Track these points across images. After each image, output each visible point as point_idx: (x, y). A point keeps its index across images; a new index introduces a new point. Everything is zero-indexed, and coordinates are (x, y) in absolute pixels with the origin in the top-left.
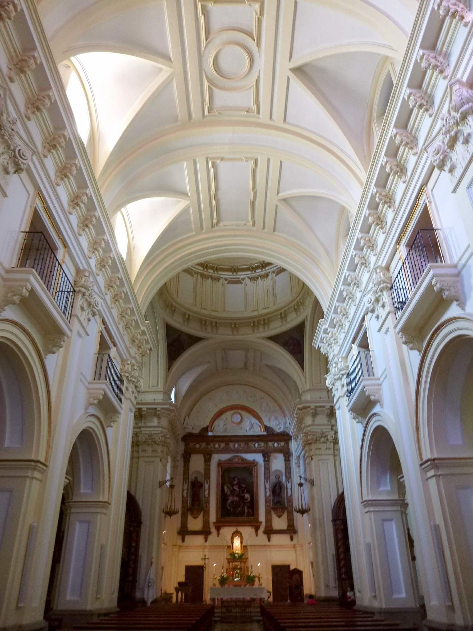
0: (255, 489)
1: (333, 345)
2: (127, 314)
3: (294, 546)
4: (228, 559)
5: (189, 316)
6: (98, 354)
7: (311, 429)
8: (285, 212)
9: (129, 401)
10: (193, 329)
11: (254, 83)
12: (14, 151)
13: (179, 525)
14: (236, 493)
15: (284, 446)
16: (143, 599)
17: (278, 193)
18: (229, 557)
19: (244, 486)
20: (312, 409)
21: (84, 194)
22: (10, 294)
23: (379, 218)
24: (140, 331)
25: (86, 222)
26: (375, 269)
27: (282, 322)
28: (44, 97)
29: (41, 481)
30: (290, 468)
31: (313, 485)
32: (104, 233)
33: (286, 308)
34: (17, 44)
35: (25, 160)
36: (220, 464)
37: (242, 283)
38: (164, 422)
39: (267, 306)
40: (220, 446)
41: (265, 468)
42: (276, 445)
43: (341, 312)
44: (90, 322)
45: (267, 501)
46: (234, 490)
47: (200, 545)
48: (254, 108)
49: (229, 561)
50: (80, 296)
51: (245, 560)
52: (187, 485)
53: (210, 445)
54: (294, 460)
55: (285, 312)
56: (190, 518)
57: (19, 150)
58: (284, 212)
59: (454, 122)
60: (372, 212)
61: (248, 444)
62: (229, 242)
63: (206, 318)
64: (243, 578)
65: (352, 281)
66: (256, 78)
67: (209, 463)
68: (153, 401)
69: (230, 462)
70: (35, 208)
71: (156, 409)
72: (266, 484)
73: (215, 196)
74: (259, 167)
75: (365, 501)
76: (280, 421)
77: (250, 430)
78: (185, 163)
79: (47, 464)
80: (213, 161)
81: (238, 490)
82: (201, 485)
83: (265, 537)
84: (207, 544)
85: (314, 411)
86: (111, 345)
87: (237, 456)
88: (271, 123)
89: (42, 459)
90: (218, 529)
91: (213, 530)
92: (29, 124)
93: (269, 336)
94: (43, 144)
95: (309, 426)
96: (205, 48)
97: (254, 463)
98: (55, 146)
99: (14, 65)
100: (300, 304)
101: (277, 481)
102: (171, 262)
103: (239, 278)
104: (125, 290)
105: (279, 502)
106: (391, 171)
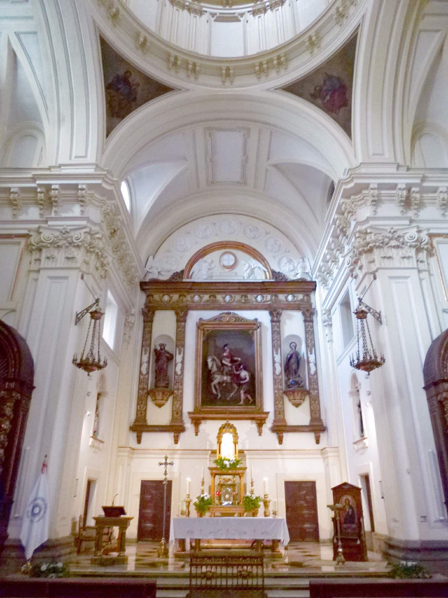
5: (145, 40)
13: (133, 417)
14: (226, 369)
15: (302, 300)
18: (214, 465)
19: (239, 359)
26: (354, 233)
30: (313, 332)
31: (381, 323)
36: (201, 325)
41: (273, 332)
45: (276, 381)
46: (223, 365)
51: (241, 471)
52: (147, 355)
53: (185, 296)
54: (319, 320)
55: (317, 33)
56: (151, 405)
61: (246, 296)
64: (237, 502)
67: (183, 324)
69: (217, 322)
72: (275, 355)
81: (229, 364)
82: (170, 358)
83: (274, 437)
84: (178, 446)
90: (197, 422)
91: (188, 425)
97: (255, 324)
101: (291, 353)
103: (234, 13)
105: (297, 383)
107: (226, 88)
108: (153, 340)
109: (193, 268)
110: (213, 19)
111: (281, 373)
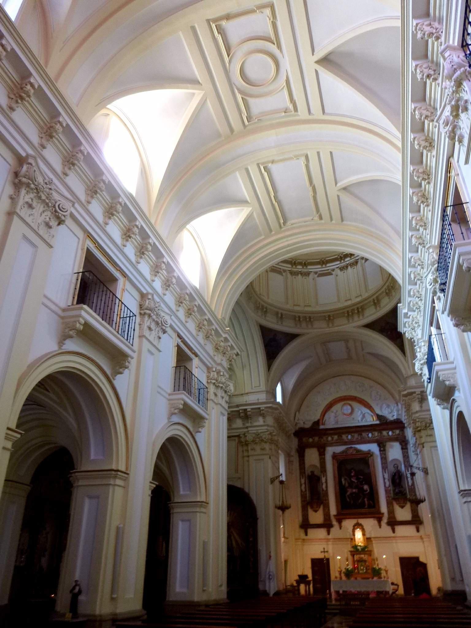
0: (373, 480)
1: (416, 328)
2: (203, 325)
3: (421, 538)
4: (351, 552)
5: (282, 315)
6: (176, 367)
7: (419, 416)
8: (347, 200)
9: (219, 406)
10: (288, 327)
11: (285, 84)
12: (54, 206)
13: (301, 519)
15: (399, 434)
16: (266, 591)
17: (336, 184)
18: (352, 549)
20: (418, 394)
21: (135, 226)
22: (67, 330)
23: (424, 196)
24: (223, 339)
25: (142, 250)
27: (376, 308)
28: (77, 153)
29: (124, 487)
32: (163, 256)
33: (377, 295)
34: (44, 115)
35: (66, 212)
36: (335, 456)
37: (332, 274)
38: (270, 420)
39: (359, 294)
40: (333, 438)
41: (382, 458)
42: (390, 433)
43: (414, 295)
44: (161, 340)
45: (387, 491)
47: (323, 538)
48: (291, 107)
49: (353, 554)
50: (146, 317)
52: (304, 479)
55: (377, 297)
56: (310, 512)
57: (59, 206)
58: (346, 199)
59: (453, 91)
60: (416, 190)
61: (361, 435)
62: (302, 239)
63: (299, 315)
65: (415, 263)
66: (285, 78)
67: (323, 457)
68: (257, 401)
69: (345, 454)
70: (88, 249)
71: (259, 408)
72: (385, 474)
73: (276, 197)
74: (310, 161)
75: (462, 491)
76: (392, 408)
77: (362, 420)
78: (237, 174)
79: (128, 472)
80: (264, 165)
81: (356, 481)
82: (318, 479)
83: (389, 529)
84: (330, 537)
85: (420, 396)
86: (192, 356)
87: (351, 448)
88: (311, 117)
89: (122, 468)
90: (340, 522)
91: (335, 523)
92: (68, 180)
93: (364, 324)
94: (86, 192)
95: (417, 412)
96: (229, 65)
97: (369, 454)
98: (96, 191)
99: (45, 133)
100: (390, 288)
101: (395, 471)
102: (248, 266)
103: (328, 270)
104: (196, 303)
106: (420, 146)
107: (329, 328)
108: (306, 469)
109: (325, 417)
110: (316, 276)
111: (389, 486)
